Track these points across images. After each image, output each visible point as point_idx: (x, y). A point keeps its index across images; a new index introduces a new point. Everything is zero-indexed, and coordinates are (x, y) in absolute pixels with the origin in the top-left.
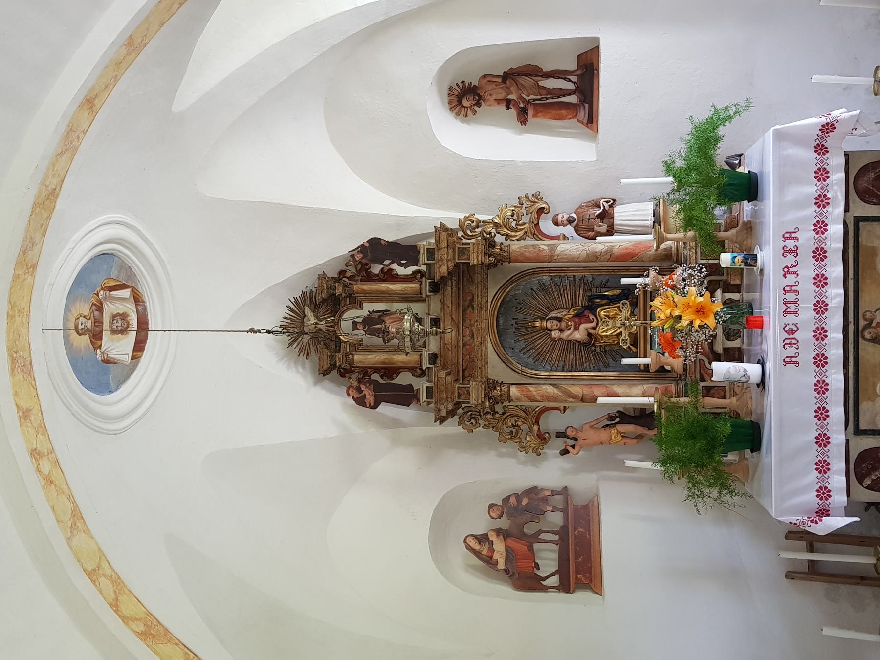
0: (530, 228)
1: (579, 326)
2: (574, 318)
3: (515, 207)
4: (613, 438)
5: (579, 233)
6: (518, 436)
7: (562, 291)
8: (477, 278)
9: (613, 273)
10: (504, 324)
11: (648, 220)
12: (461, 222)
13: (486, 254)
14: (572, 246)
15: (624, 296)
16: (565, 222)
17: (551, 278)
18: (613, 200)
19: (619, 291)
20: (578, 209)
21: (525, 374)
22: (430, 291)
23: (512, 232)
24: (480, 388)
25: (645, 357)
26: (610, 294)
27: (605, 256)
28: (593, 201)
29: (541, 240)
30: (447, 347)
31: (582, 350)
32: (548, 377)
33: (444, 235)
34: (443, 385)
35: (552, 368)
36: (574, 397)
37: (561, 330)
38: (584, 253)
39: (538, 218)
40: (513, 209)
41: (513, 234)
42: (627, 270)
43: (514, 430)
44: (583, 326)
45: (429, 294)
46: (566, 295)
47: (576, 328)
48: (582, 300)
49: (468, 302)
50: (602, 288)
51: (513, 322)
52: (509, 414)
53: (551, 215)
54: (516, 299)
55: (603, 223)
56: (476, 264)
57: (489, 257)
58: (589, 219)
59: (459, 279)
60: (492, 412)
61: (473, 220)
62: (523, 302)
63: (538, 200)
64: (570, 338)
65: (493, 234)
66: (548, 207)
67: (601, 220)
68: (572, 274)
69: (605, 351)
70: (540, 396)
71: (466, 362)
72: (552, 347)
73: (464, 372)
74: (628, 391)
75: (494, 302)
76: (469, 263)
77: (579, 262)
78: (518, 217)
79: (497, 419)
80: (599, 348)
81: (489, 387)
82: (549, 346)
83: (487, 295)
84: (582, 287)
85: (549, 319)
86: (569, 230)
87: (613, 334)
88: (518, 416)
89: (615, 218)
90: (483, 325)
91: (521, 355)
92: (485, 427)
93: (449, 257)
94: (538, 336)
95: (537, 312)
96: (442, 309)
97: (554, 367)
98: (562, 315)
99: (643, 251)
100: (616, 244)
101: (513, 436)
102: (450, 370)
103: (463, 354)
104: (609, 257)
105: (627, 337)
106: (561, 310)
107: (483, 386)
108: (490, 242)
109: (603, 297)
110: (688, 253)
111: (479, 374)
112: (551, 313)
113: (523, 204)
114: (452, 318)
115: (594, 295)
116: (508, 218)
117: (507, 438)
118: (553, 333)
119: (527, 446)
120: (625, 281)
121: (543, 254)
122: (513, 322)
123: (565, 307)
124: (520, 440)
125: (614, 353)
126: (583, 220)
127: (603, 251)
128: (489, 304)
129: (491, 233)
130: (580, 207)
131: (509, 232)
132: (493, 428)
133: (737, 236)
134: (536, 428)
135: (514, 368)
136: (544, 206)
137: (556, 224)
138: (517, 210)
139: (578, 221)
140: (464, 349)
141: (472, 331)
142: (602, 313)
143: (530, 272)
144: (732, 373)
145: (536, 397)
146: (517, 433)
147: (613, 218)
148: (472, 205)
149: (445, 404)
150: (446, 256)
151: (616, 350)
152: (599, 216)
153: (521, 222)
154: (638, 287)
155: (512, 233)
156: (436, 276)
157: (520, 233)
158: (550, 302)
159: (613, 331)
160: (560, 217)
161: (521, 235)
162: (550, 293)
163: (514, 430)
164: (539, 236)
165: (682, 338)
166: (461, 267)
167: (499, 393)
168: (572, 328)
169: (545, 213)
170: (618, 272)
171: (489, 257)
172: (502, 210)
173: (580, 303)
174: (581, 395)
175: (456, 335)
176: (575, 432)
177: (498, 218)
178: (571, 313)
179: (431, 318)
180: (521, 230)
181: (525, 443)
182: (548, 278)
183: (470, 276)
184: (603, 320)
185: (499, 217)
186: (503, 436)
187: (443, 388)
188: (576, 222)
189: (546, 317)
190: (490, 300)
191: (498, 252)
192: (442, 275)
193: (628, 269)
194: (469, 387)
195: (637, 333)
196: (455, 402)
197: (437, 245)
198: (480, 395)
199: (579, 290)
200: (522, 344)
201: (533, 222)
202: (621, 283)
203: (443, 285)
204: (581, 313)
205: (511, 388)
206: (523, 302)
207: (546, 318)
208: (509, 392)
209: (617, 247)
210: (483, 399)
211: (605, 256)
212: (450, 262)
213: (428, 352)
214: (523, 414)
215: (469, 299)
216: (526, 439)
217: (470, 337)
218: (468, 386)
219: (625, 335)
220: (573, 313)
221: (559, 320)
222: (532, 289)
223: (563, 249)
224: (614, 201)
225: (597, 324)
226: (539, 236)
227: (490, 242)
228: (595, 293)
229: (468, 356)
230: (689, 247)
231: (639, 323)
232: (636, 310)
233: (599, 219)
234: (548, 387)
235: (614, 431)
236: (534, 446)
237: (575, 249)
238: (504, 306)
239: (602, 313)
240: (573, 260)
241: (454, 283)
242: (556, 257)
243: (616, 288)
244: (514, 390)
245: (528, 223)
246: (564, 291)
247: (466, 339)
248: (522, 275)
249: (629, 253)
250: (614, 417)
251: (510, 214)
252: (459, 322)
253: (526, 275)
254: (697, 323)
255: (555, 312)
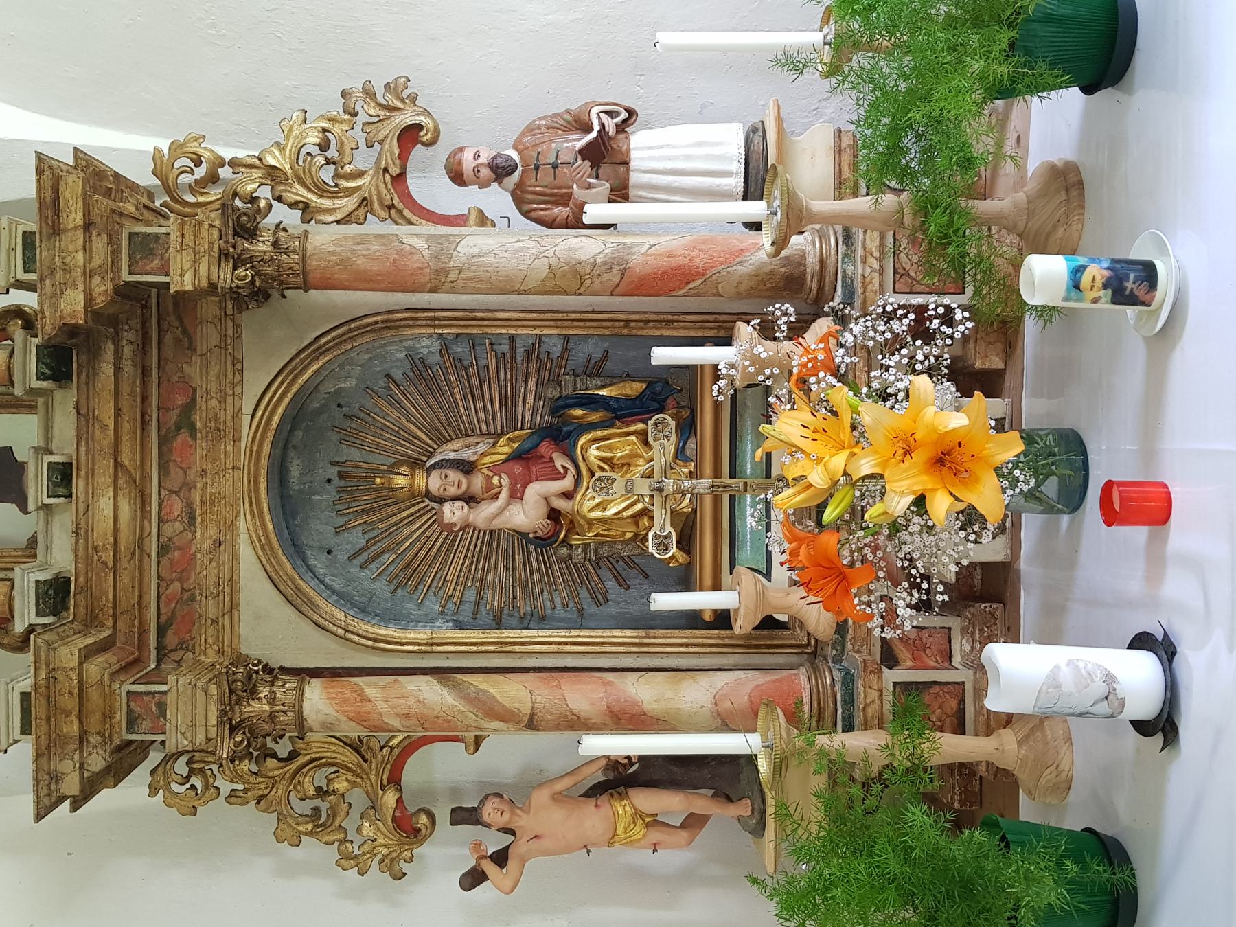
0: (377, 187)
1: (525, 487)
2: (510, 464)
3: (332, 120)
4: (619, 832)
5: (526, 207)
6: (337, 823)
7: (475, 384)
8: (208, 337)
9: (625, 332)
10: (305, 479)
11: (727, 174)
12: (158, 163)
13: (223, 255)
14: (503, 241)
15: (652, 399)
16: (485, 172)
17: (445, 347)
18: (627, 110)
19: (638, 387)
20: (523, 134)
21: (355, 638)
22: (41, 376)
23: (321, 197)
24: (200, 696)
25: (716, 587)
26: (614, 394)
27: (606, 277)
28: (568, 112)
29: (411, 223)
30: (99, 558)
31: (533, 555)
32: (429, 648)
33: (72, 189)
34: (70, 693)
35: (444, 608)
36: (506, 716)
37: (470, 499)
38: (541, 267)
39: (403, 157)
40: (326, 125)
41: (325, 203)
42: (668, 323)
43: (324, 806)
44: (536, 490)
45: (36, 384)
46: (487, 396)
47: (516, 495)
48: (534, 409)
49: (177, 411)
50: (590, 376)
51: (332, 472)
52: (308, 758)
53: (441, 152)
54: (339, 405)
55: (597, 177)
56: (189, 288)
57: (235, 268)
58: (555, 166)
59: (146, 337)
60: (255, 754)
61: (200, 156)
62: (362, 415)
63: (404, 102)
64: (496, 524)
65: (263, 204)
66: (431, 125)
67: (592, 167)
68: (504, 331)
69: (598, 559)
70: (397, 715)
71: (170, 601)
72: (444, 548)
73: (164, 636)
74: (670, 694)
75: (259, 414)
76: (168, 283)
77: (525, 293)
78: (341, 152)
79: (271, 774)
80: (580, 551)
81: (231, 692)
82: (438, 545)
83: (238, 390)
84: (533, 374)
85: (433, 467)
86: (497, 200)
87: (625, 514)
88: (335, 765)
89: (633, 164)
90: (225, 486)
91: (355, 570)
92: (233, 800)
93: (96, 262)
94: (406, 513)
95: (402, 446)
96: (84, 434)
97: (450, 605)
98: (474, 453)
99: (722, 264)
100: (639, 239)
101: (319, 824)
102: (107, 633)
103: (159, 577)
104: (617, 280)
105: (669, 529)
106: (473, 440)
107: (213, 689)
108: (239, 217)
109: (591, 402)
110: (860, 271)
111: (210, 640)
112: (444, 447)
113: (356, 114)
114: (118, 465)
115: (568, 397)
116: (309, 154)
117: (301, 832)
118: (447, 507)
119: (364, 854)
120: (663, 355)
121: (413, 264)
122: (332, 472)
123: (484, 429)
124: (342, 835)
125: (621, 563)
126: (537, 168)
127: (599, 261)
128: (246, 420)
129: (257, 198)
130: (530, 130)
131: (311, 196)
132: (258, 803)
133: (1030, 213)
134: (390, 798)
135: (321, 621)
136: (420, 119)
137: (458, 178)
138: (336, 129)
139: (523, 172)
140: (164, 561)
141: (189, 505)
142: (593, 452)
143: (377, 323)
144: (1064, 689)
145: (385, 719)
146: (333, 813)
147: (626, 163)
148: (203, 115)
149: (77, 756)
150: (80, 256)
151: (628, 556)
152: (586, 153)
153: (348, 169)
154: (724, 371)
155: (323, 201)
156: (44, 325)
157: (347, 204)
158: (442, 416)
159: (623, 505)
160: (468, 156)
161: (351, 208)
162: (440, 389)
163: (324, 806)
164: (406, 213)
165: (874, 552)
166: (154, 300)
167: (267, 708)
168: (504, 495)
169: (424, 144)
170: (640, 328)
171: (235, 268)
172: (291, 129)
173: (528, 418)
174: (526, 710)
175: (134, 519)
176: (506, 816)
177: (277, 153)
178: (500, 450)
179: (50, 464)
180: (349, 192)
181: (358, 840)
182: (436, 345)
183: (185, 331)
184: (598, 474)
185: (282, 150)
186: (290, 825)
187: (70, 703)
188: (517, 174)
189: (429, 458)
190: (248, 408)
191: (265, 252)
192: (68, 321)
193: (668, 319)
194: (165, 693)
195: (695, 511)
196: (117, 742)
197: (43, 218)
198: (200, 720)
199: (526, 381)
200: (357, 538)
201: (386, 170)
202: (654, 362)
203: (84, 358)
204: (530, 449)
205: (308, 693)
206: (362, 415)
207: (428, 465)
208: (301, 707)
209: (643, 250)
210: (213, 732)
211: (606, 277)
212: (97, 280)
213: (34, 577)
214: (349, 757)
215: (180, 403)
216: (359, 830)
217: (183, 522)
218: (164, 688)
219: (663, 525)
220: (507, 450)
221: (467, 468)
222: (388, 376)
223: (475, 251)
224: (631, 113)
225: (578, 481)
226: (406, 213)
227: (239, 217)
228: (569, 391)
229: (177, 585)
230: (860, 252)
231: (704, 484)
232: (691, 444)
233: (587, 163)
234: (424, 687)
235: (623, 809)
236: (385, 851)
237: (516, 251)
238: (304, 425)
239: (593, 452)
240: (507, 288)
241: (127, 351)
242: (453, 275)
243: (629, 377)
244: (317, 700)
245: (371, 172)
246: (481, 382)
247: (168, 530)
248: (350, 331)
249: (679, 267)
250: (624, 765)
251: (317, 140)
252: (146, 476)
253: (363, 331)
254: (941, 506)
255: (457, 444)
